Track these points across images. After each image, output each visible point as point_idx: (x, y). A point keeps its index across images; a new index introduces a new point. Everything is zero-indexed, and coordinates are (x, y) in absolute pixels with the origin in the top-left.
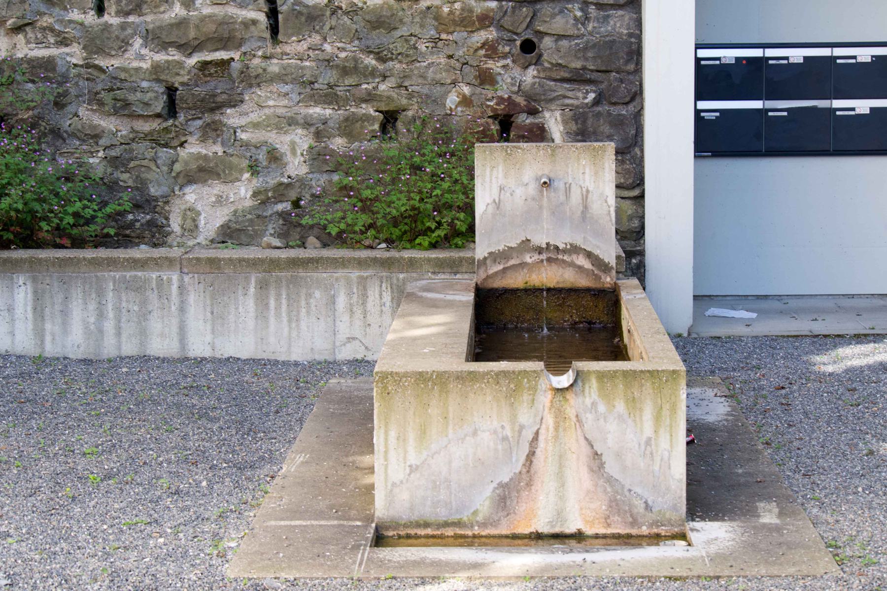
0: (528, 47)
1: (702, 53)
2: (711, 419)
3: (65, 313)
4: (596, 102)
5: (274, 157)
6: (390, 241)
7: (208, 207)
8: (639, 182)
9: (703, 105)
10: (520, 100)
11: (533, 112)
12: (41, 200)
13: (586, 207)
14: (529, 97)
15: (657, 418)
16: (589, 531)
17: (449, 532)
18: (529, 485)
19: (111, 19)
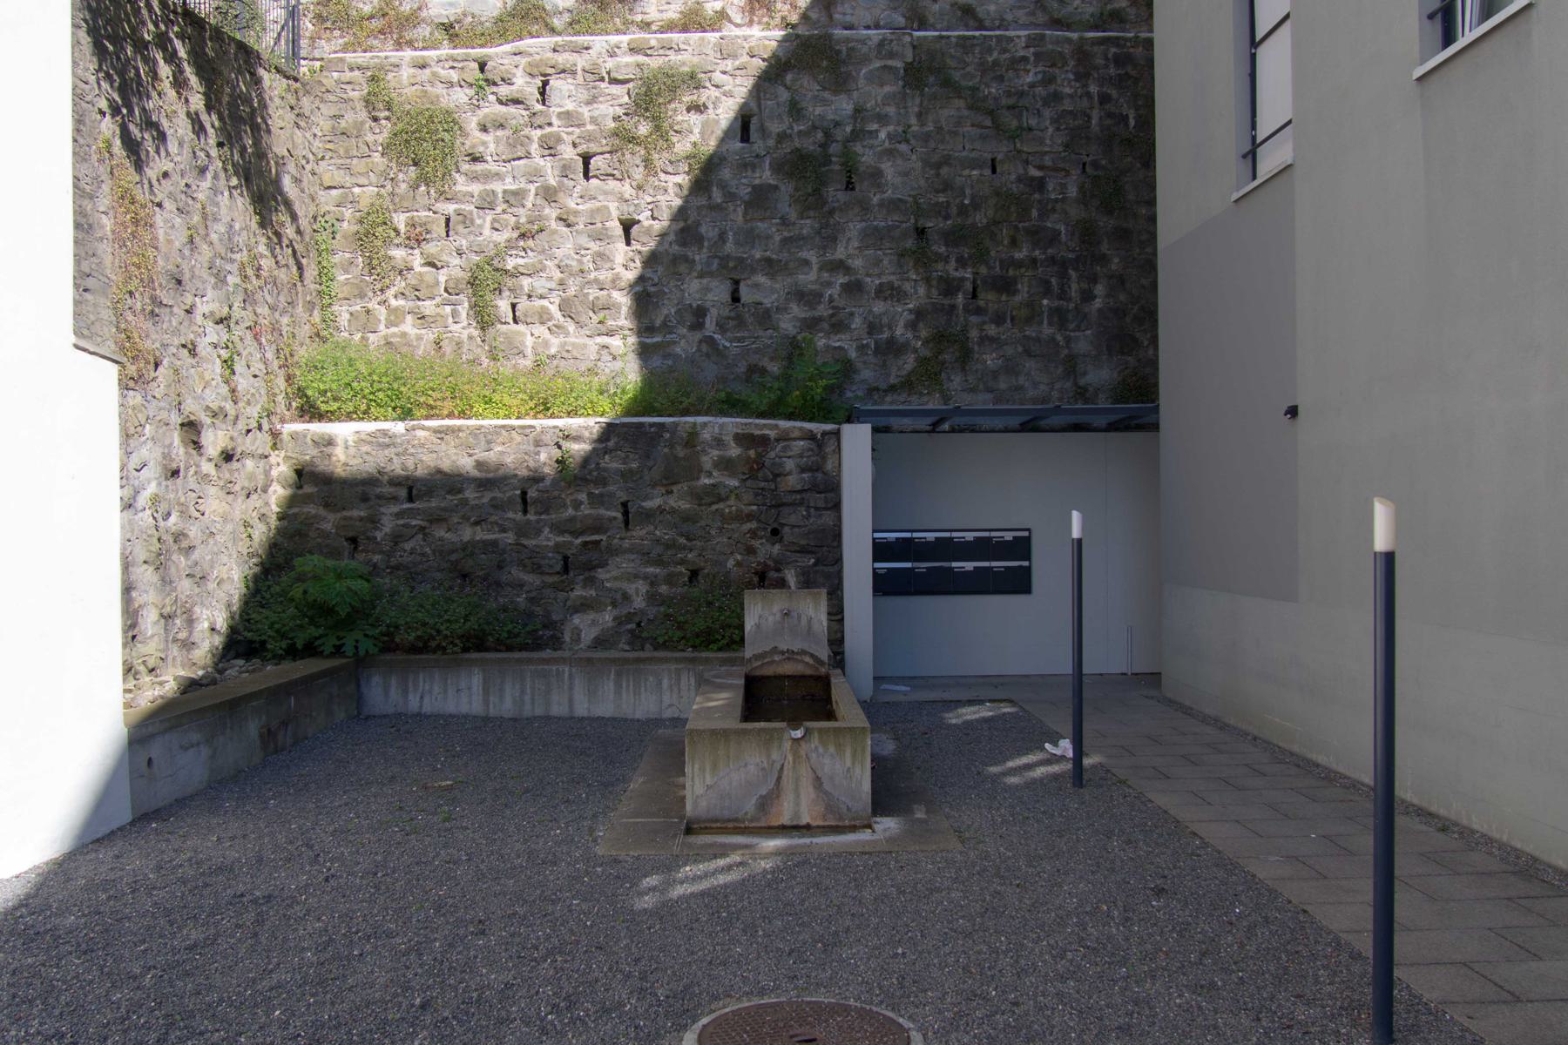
0: (775, 532)
1: (877, 535)
2: (885, 753)
3: (501, 690)
4: (815, 564)
5: (626, 597)
6: (694, 647)
7: (587, 626)
8: (841, 611)
9: (877, 565)
10: (770, 563)
11: (778, 570)
12: (489, 623)
13: (810, 628)
14: (776, 562)
15: (854, 755)
16: (814, 824)
17: (730, 825)
18: (778, 797)
19: (531, 517)
